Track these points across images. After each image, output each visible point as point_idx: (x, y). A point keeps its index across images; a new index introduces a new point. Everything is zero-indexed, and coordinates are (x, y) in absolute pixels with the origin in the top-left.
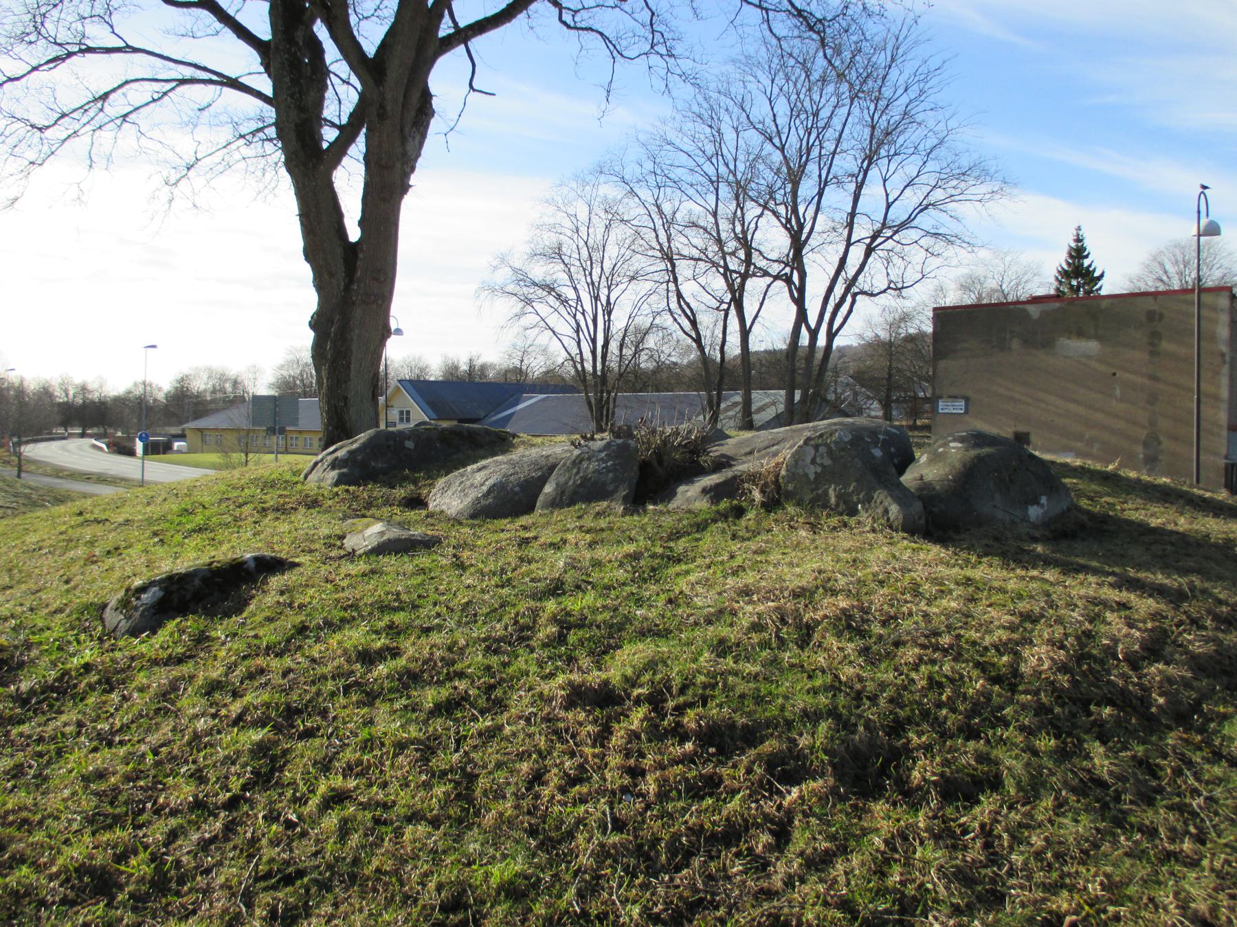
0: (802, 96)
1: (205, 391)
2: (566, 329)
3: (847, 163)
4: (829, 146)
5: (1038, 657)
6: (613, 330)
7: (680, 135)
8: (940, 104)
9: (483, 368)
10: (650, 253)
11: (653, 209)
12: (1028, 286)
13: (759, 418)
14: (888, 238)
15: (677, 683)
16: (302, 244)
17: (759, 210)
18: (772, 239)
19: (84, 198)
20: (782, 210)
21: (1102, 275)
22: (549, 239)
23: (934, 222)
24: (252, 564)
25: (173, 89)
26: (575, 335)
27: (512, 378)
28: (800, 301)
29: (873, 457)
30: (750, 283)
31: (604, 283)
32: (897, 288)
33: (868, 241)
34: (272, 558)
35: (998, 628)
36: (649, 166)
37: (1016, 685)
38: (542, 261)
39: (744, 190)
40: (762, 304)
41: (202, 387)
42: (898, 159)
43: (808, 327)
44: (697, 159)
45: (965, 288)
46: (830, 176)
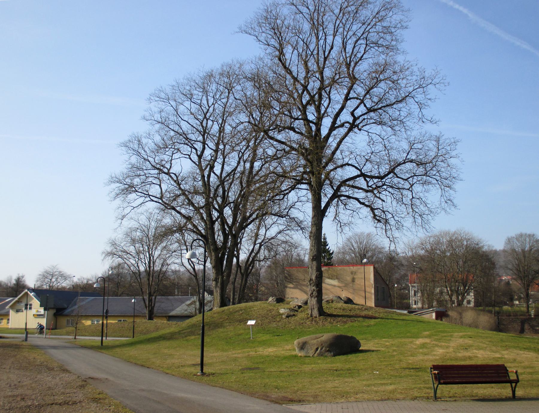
21: (333, 252)
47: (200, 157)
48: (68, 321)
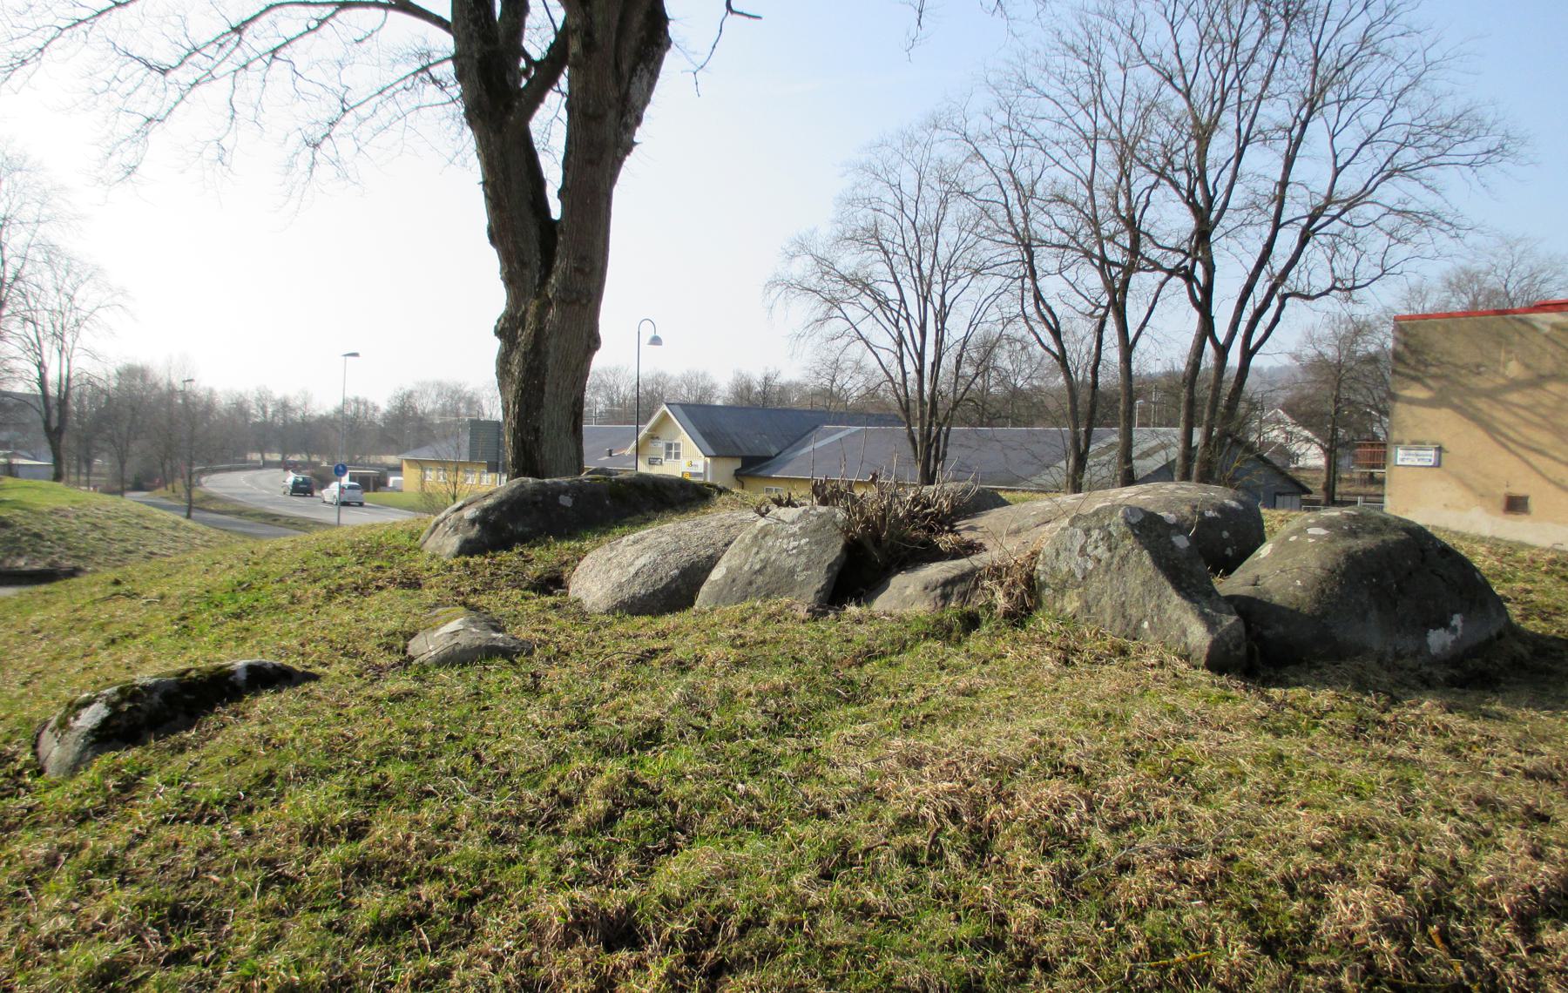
0: (1217, 19)
1: (433, 412)
2: (883, 339)
3: (1276, 112)
4: (1254, 88)
5: (1353, 907)
6: (948, 340)
7: (1045, 75)
8: (1415, 27)
9: (784, 390)
10: (999, 237)
11: (1005, 176)
12: (1547, 287)
13: (1142, 466)
14: (1334, 218)
15: (743, 911)
16: (486, 222)
17: (1152, 178)
18: (1169, 219)
19: (226, 159)
20: (1183, 178)
22: (864, 217)
23: (1400, 194)
24: (242, 676)
25: (333, 15)
26: (895, 348)
27: (820, 403)
28: (1204, 307)
29: (1173, 547)
30: (1135, 280)
31: (937, 278)
32: (1345, 288)
33: (1305, 221)
34: (275, 666)
35: (1301, 847)
36: (1001, 117)
37: (1303, 955)
38: (854, 248)
39: (1132, 149)
40: (1151, 310)
41: (429, 407)
42: (1353, 105)
43: (1215, 341)
44: (1067, 108)
45: (1455, 286)
46: (1254, 129)
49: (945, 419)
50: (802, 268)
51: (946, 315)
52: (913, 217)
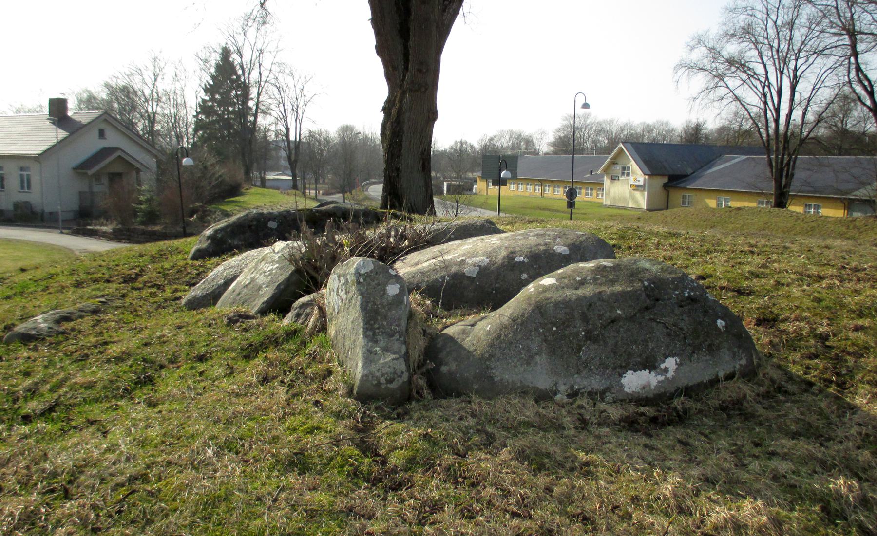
1: (508, 147)
22: (741, 20)
26: (762, 106)
47: (775, 23)
48: (684, 197)
49: (794, 152)
50: (699, 54)
51: (797, 82)
52: (774, 18)
